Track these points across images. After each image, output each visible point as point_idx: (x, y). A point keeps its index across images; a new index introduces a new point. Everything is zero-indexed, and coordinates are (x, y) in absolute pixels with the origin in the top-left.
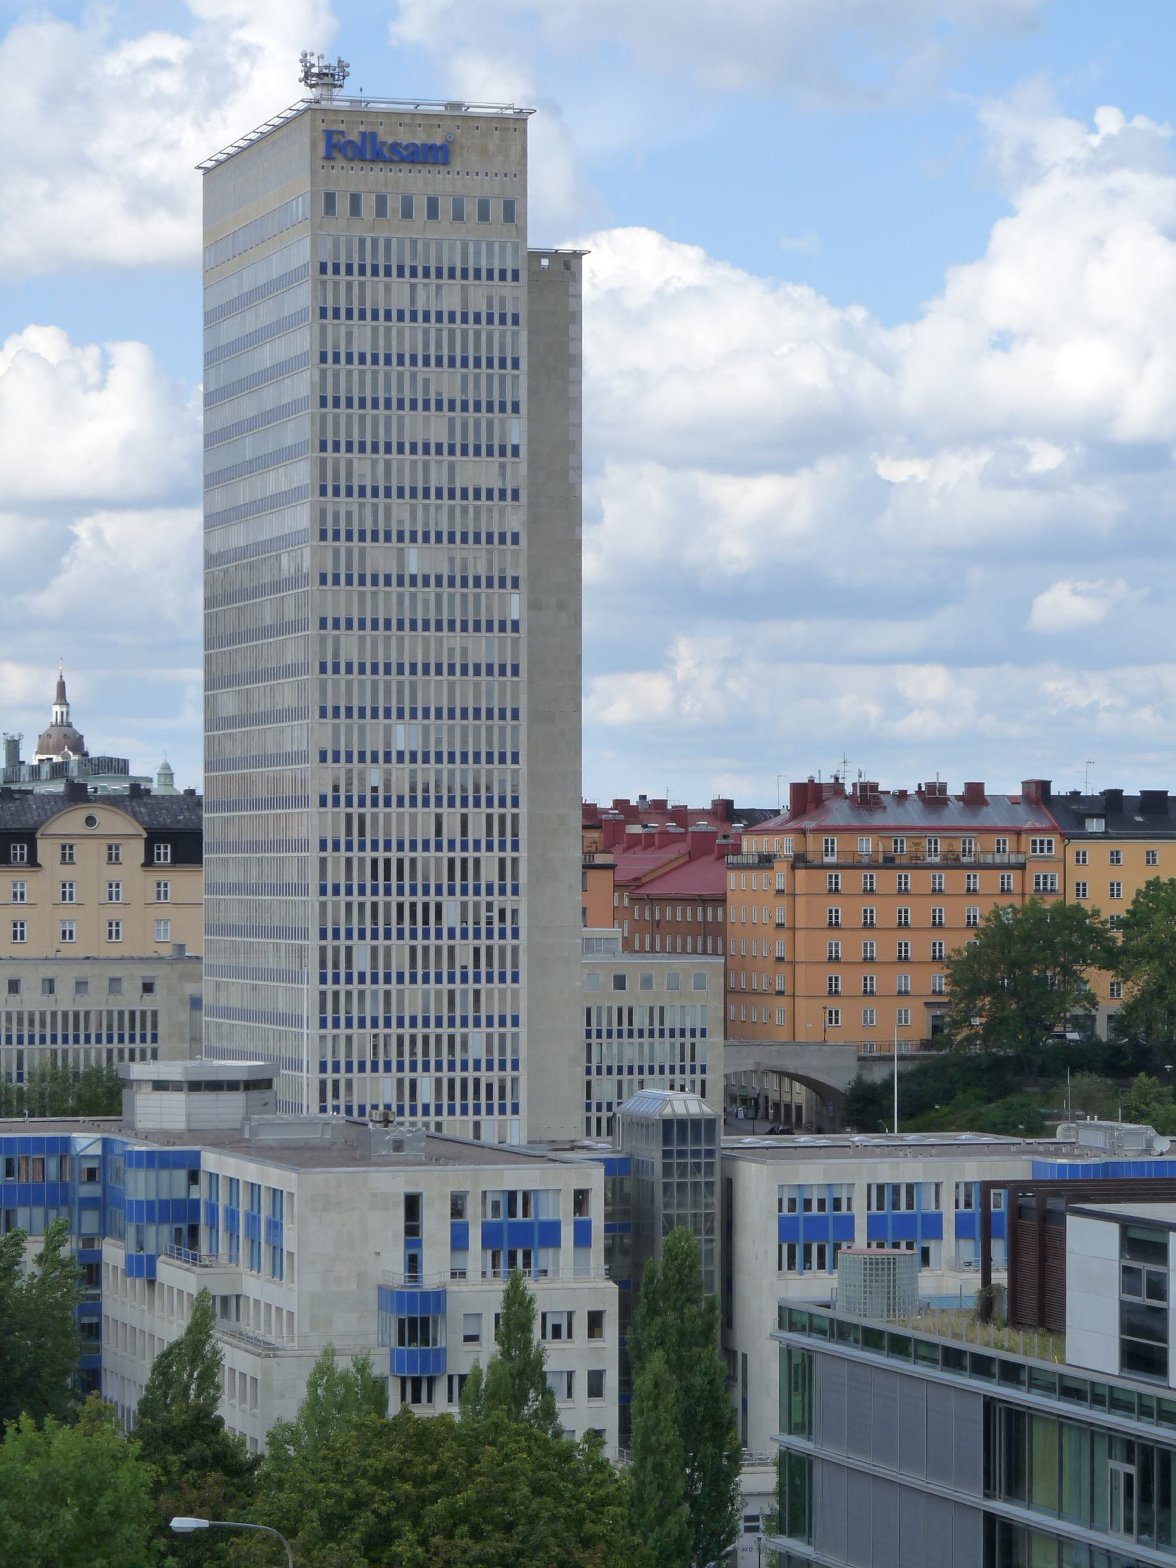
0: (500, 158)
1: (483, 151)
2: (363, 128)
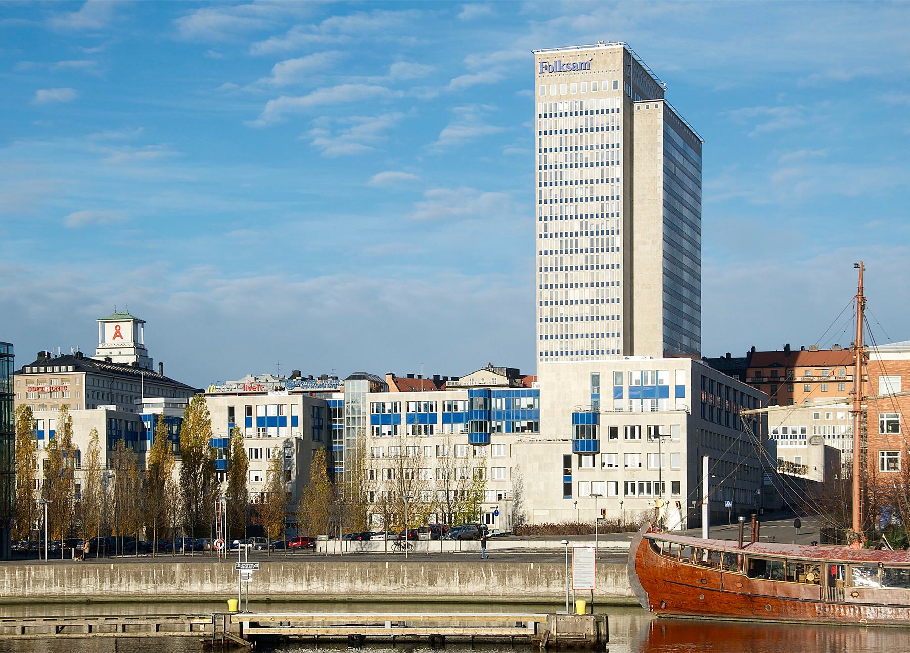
1: (605, 62)
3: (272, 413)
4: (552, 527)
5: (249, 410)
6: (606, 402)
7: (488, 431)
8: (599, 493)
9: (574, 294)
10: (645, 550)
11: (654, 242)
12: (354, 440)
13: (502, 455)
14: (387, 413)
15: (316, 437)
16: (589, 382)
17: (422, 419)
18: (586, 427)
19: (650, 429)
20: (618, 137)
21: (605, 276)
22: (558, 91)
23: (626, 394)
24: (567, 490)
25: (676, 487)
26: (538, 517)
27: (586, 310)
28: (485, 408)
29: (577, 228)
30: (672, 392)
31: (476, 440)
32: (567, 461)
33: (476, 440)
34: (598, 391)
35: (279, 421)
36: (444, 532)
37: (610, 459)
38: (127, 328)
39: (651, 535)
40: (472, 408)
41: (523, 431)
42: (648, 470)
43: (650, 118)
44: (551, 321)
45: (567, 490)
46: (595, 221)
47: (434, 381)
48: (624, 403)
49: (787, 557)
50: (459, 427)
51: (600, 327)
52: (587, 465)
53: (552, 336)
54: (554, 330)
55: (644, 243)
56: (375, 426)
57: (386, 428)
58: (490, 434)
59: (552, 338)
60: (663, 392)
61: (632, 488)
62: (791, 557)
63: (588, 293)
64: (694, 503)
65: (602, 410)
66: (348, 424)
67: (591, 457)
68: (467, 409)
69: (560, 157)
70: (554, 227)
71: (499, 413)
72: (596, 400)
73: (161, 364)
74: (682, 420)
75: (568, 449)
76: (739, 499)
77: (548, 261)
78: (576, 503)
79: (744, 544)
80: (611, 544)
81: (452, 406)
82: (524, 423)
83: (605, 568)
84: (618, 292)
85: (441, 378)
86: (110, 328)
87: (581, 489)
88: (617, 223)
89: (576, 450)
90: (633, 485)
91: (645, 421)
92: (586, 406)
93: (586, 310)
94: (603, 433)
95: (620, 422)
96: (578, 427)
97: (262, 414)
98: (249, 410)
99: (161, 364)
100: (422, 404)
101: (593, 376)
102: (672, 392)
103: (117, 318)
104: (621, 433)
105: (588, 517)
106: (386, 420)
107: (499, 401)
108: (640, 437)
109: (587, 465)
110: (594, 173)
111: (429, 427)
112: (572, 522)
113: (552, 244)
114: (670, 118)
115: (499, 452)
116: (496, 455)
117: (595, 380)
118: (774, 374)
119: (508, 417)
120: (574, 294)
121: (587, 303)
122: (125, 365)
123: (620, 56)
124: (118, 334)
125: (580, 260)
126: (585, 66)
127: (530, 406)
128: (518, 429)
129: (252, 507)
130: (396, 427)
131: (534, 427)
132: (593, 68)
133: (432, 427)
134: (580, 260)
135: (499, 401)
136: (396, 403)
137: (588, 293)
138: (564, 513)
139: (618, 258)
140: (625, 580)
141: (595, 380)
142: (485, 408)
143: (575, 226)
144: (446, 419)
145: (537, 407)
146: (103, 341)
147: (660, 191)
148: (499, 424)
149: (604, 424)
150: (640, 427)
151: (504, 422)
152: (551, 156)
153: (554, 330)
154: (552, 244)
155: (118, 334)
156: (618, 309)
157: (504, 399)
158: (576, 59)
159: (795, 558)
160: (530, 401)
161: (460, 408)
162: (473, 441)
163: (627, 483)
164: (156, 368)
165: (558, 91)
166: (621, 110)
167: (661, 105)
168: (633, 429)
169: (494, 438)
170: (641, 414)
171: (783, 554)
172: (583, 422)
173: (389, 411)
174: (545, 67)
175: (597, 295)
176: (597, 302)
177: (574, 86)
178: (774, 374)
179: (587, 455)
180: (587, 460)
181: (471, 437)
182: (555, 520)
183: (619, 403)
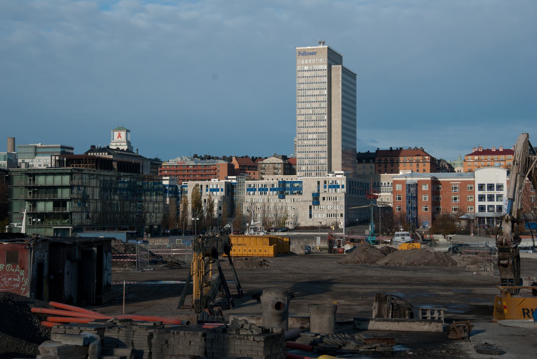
3: (215, 187)
5: (207, 186)
6: (322, 189)
8: (320, 217)
9: (310, 136)
11: (338, 117)
16: (317, 183)
17: (263, 190)
20: (326, 79)
21: (321, 130)
23: (327, 187)
24: (311, 216)
25: (342, 215)
26: (303, 224)
29: (311, 112)
32: (310, 207)
35: (217, 190)
36: (277, 230)
38: (123, 134)
42: (333, 210)
43: (337, 70)
45: (311, 216)
48: (327, 189)
50: (275, 192)
51: (319, 149)
55: (335, 117)
57: (252, 193)
60: (338, 187)
63: (315, 136)
69: (305, 86)
70: (303, 111)
71: (288, 188)
73: (137, 150)
74: (343, 195)
75: (311, 204)
77: (301, 124)
80: (323, 233)
82: (296, 192)
86: (116, 134)
87: (315, 216)
88: (325, 111)
89: (313, 204)
91: (333, 195)
94: (321, 199)
97: (211, 187)
98: (207, 186)
99: (137, 150)
103: (120, 129)
104: (326, 199)
105: (317, 224)
106: (252, 190)
110: (317, 92)
113: (302, 118)
114: (345, 71)
117: (319, 183)
118: (386, 160)
122: (123, 150)
123: (326, 51)
124: (119, 136)
125: (312, 124)
126: (314, 53)
129: (216, 218)
132: (317, 54)
134: (312, 124)
137: (315, 136)
138: (309, 223)
139: (325, 123)
140: (326, 243)
141: (319, 183)
144: (271, 190)
146: (113, 139)
147: (341, 98)
152: (302, 86)
154: (302, 118)
155: (119, 136)
156: (326, 142)
162: (279, 198)
164: (135, 151)
169: (286, 196)
174: (300, 53)
177: (310, 61)
178: (386, 160)
180: (316, 207)
183: (326, 190)
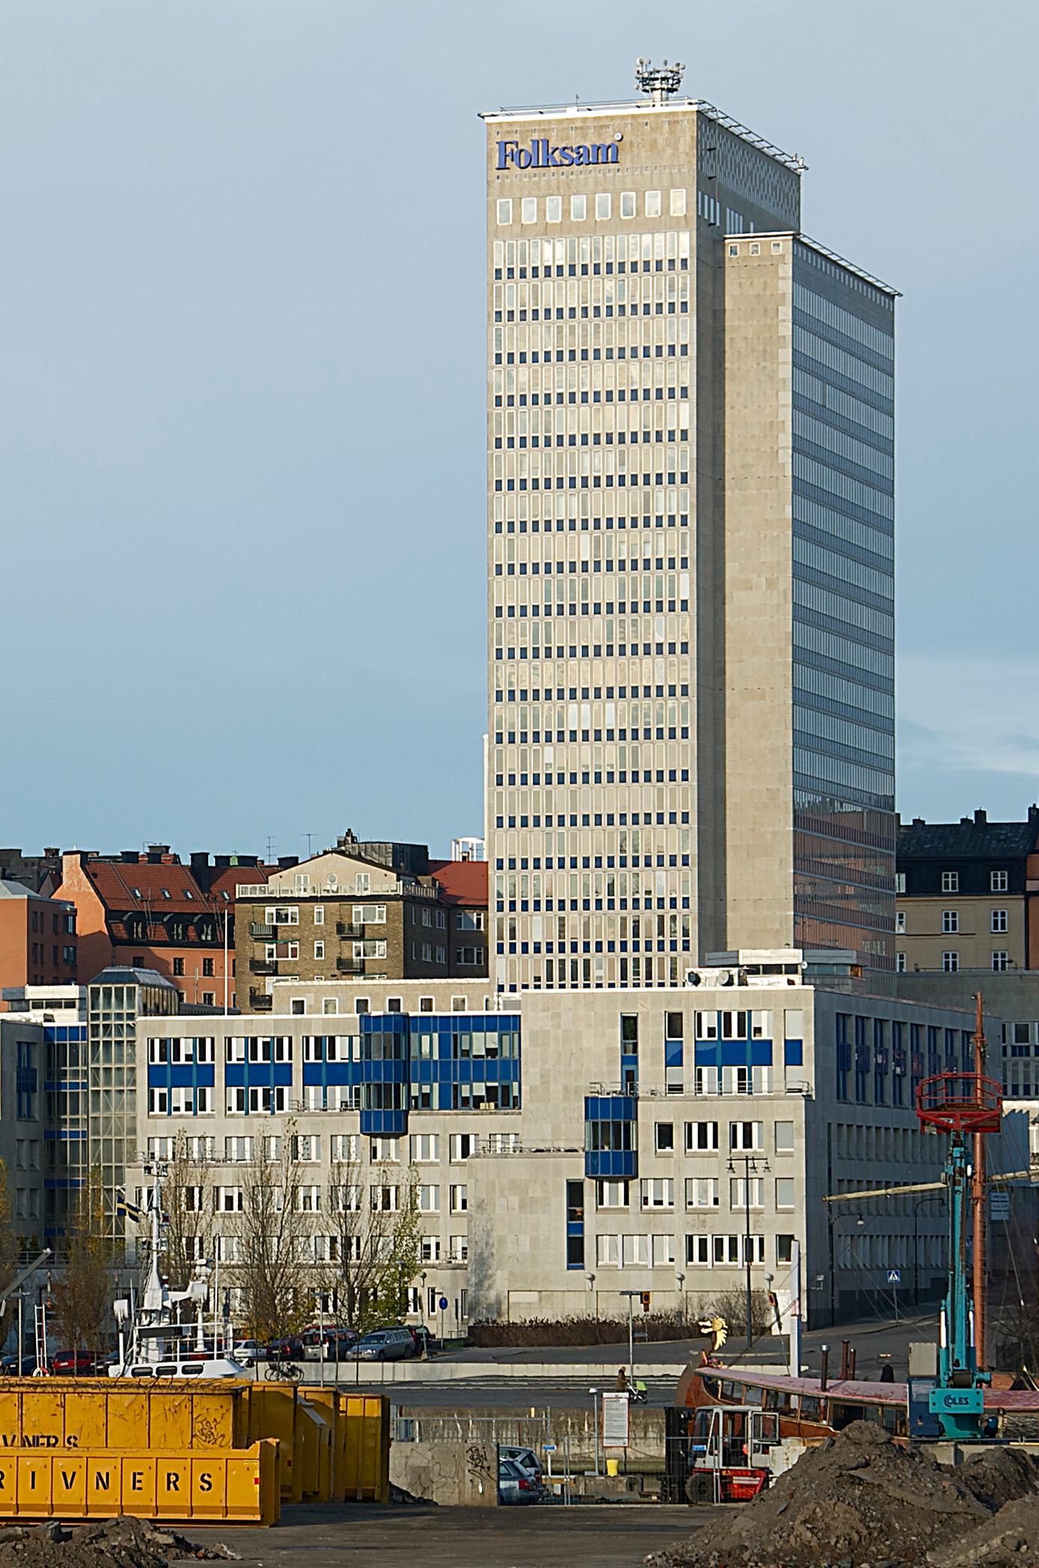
0: (669, 151)
1: (653, 146)
2: (536, 137)
4: (546, 1326)
6: (651, 1071)
7: (404, 1107)
8: (640, 1260)
9: (578, 715)
10: (698, 1393)
11: (771, 585)
12: (107, 1119)
13: (432, 1158)
14: (183, 1061)
15: (25, 1110)
17: (258, 1074)
18: (611, 1122)
19: (735, 1128)
20: (684, 330)
21: (654, 671)
22: (541, 212)
23: (689, 1058)
24: (576, 1254)
27: (609, 756)
28: (397, 1055)
30: (779, 1053)
31: (377, 1126)
32: (575, 1191)
33: (377, 1126)
34: (635, 1050)
37: (658, 1190)
39: (706, 1370)
40: (368, 1055)
41: (477, 1107)
43: (760, 267)
44: (524, 782)
45: (576, 1254)
46: (629, 535)
47: (192, 869)
49: (884, 1401)
50: (339, 1093)
51: (642, 798)
52: (614, 1199)
53: (524, 820)
54: (531, 805)
55: (748, 586)
56: (157, 1091)
57: (181, 1096)
58: (406, 1113)
59: (524, 824)
60: (762, 1053)
61: (697, 1249)
62: (888, 1401)
63: (612, 715)
64: (821, 1278)
65: (642, 1090)
66: (96, 1083)
67: (621, 1185)
68: (356, 1054)
71: (426, 1064)
72: (630, 1067)
74: (796, 1112)
75: (576, 1168)
76: (927, 1258)
78: (593, 1278)
79: (829, 1383)
81: (324, 1045)
82: (480, 1089)
83: (645, 1415)
84: (683, 712)
85: (212, 863)
87: (602, 1251)
90: (703, 1243)
92: (612, 1084)
93: (609, 756)
94: (644, 1138)
95: (673, 1112)
96: (595, 1125)
100: (260, 1042)
101: (625, 1019)
102: (779, 1053)
104: (678, 1137)
106: (181, 1077)
107: (426, 1039)
108: (715, 1146)
109: (614, 1199)
111: (274, 1093)
112: (585, 1317)
115: (426, 1153)
116: (418, 1159)
117: (630, 1027)
119: (445, 1076)
120: (578, 715)
121: (610, 737)
123: (688, 132)
127: (491, 1052)
128: (465, 1100)
130: (203, 1093)
131: (504, 1099)
133: (280, 1092)
134: (594, 630)
135: (426, 1039)
136: (203, 1041)
137: (612, 715)
138: (569, 1299)
141: (630, 1027)
142: (397, 1055)
143: (583, 547)
144: (311, 1076)
145: (506, 1054)
148: (426, 1089)
149: (648, 1116)
150: (715, 1125)
151: (436, 1085)
153: (531, 805)
156: (684, 754)
157: (436, 1035)
158: (585, 137)
159: (893, 1402)
160: (492, 1039)
161: (341, 1054)
163: (690, 1238)
165: (541, 212)
166: (692, 264)
167: (782, 246)
168: (702, 1127)
169: (415, 1121)
170: (719, 1099)
171: (880, 1397)
172: (605, 1115)
173: (188, 1057)
175: (635, 719)
176: (635, 737)
177: (578, 201)
179: (611, 1180)
181: (366, 1117)
182: (550, 1314)
183: (676, 1076)
